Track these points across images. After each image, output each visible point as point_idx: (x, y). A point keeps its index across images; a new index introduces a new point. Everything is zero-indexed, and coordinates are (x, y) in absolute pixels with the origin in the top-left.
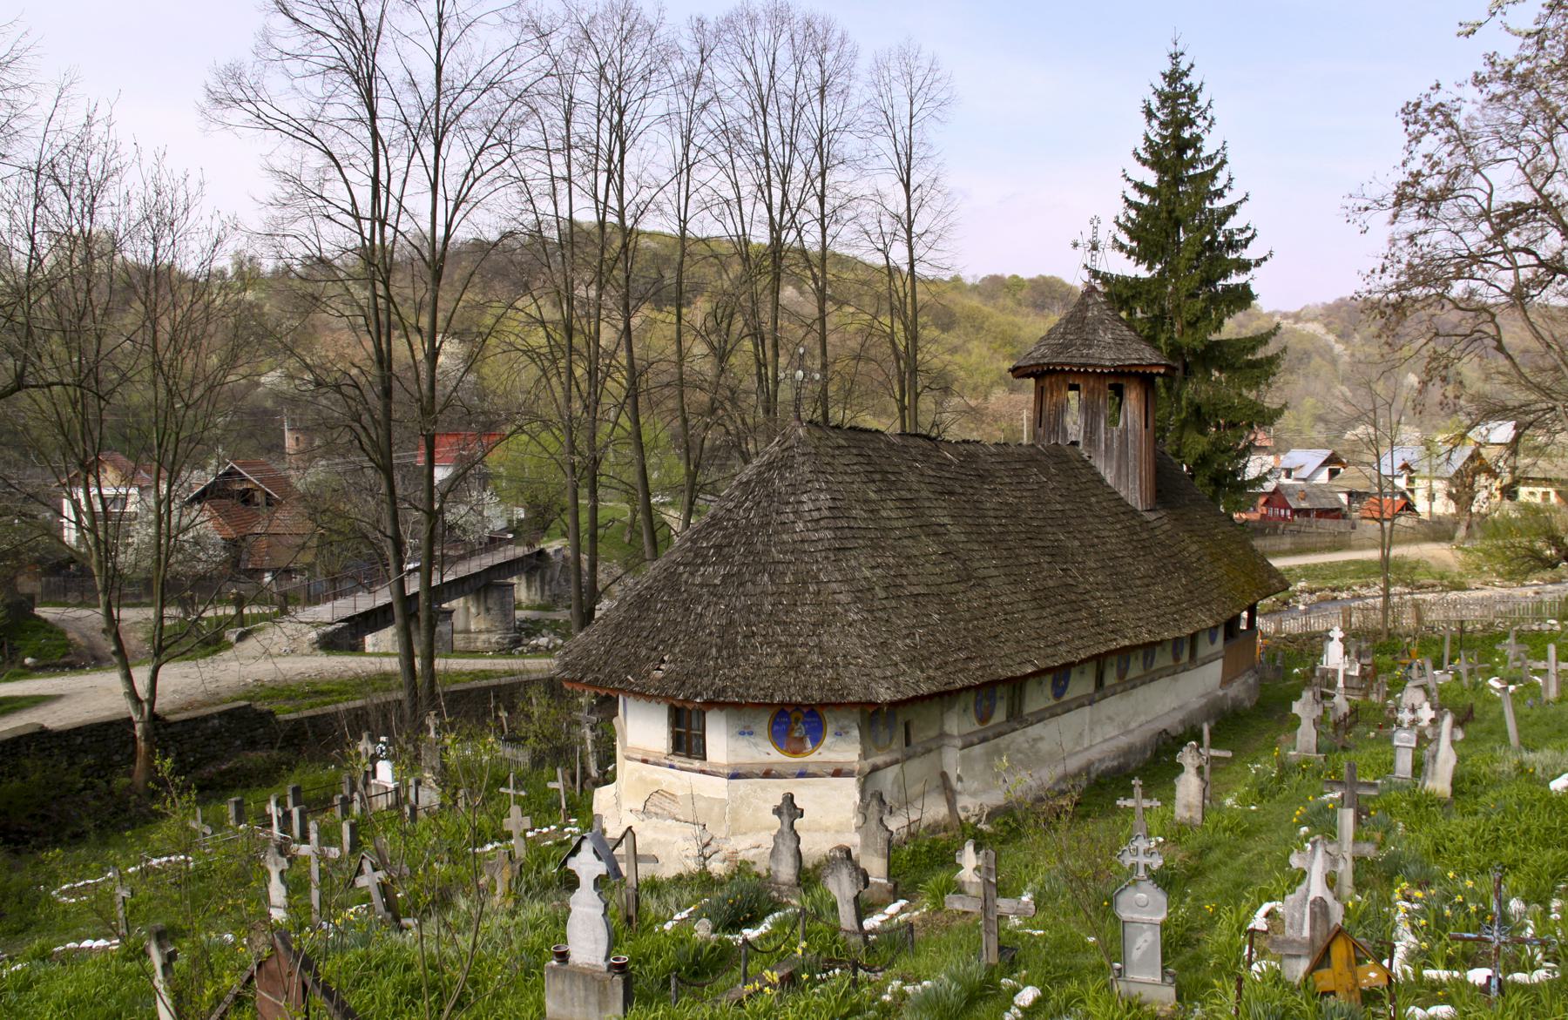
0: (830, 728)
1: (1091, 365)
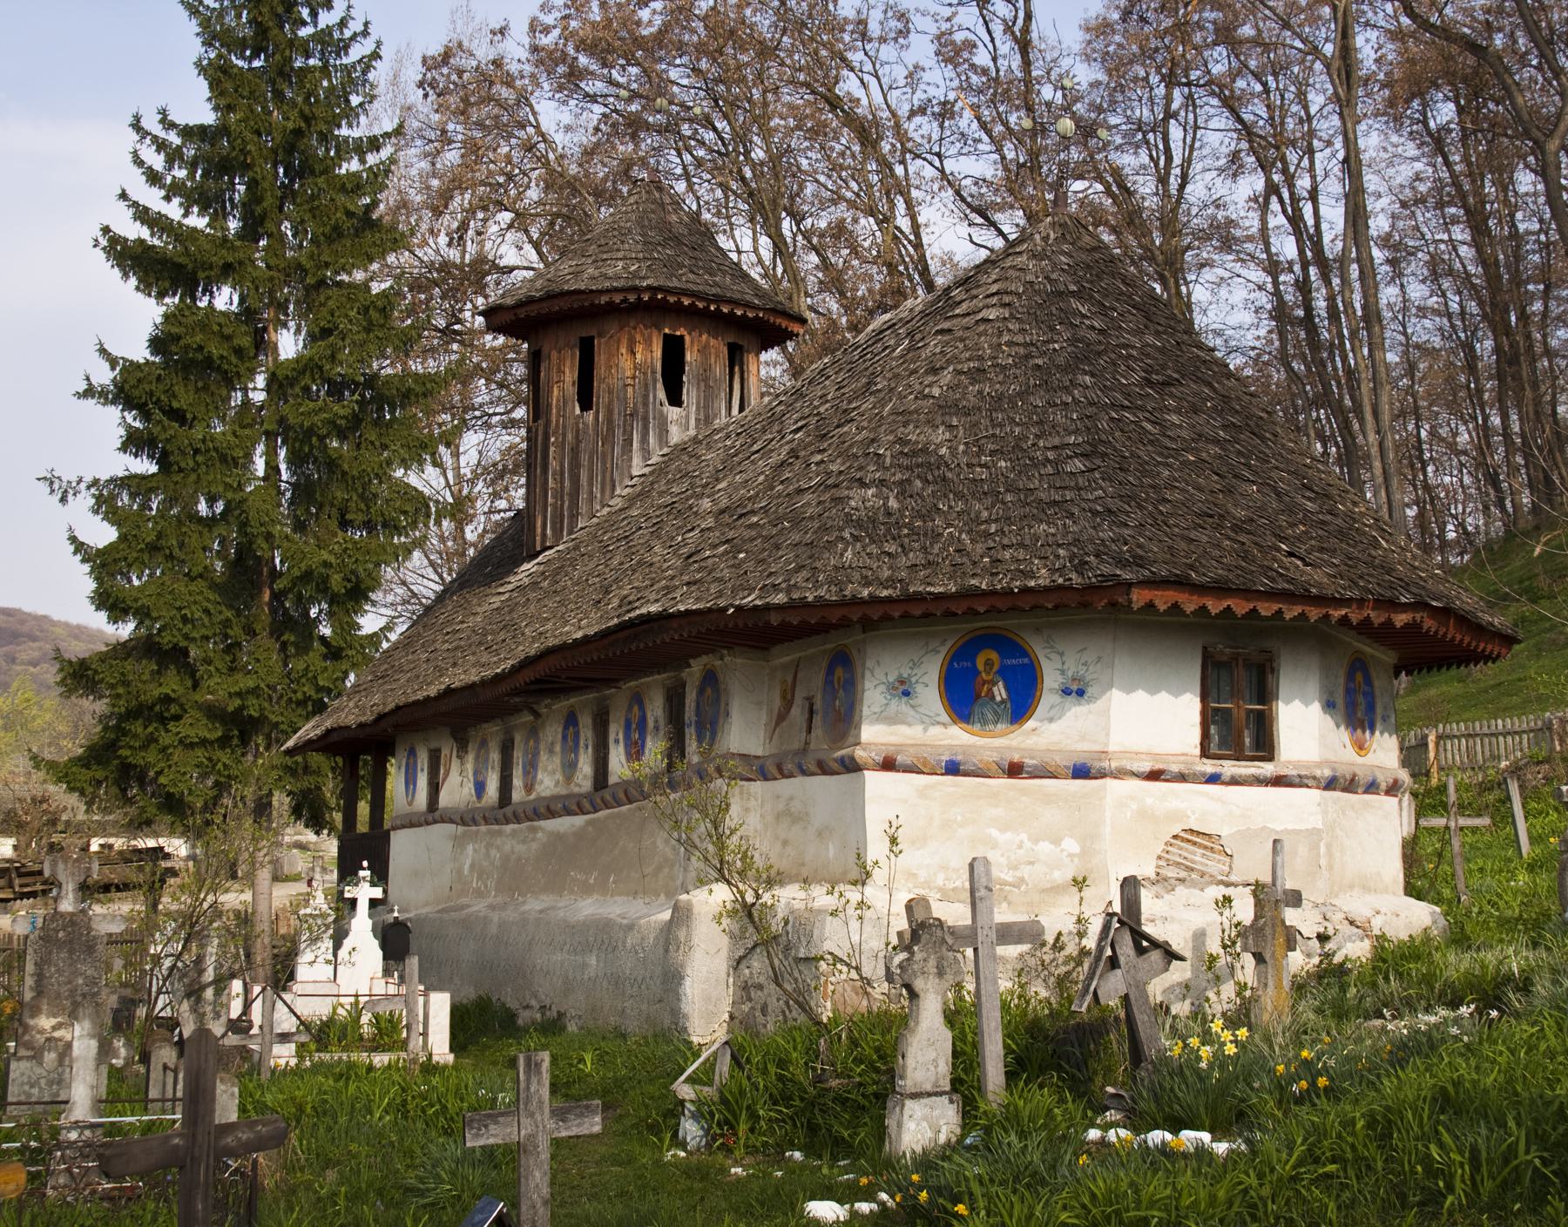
0: (1051, 679)
1: (730, 301)
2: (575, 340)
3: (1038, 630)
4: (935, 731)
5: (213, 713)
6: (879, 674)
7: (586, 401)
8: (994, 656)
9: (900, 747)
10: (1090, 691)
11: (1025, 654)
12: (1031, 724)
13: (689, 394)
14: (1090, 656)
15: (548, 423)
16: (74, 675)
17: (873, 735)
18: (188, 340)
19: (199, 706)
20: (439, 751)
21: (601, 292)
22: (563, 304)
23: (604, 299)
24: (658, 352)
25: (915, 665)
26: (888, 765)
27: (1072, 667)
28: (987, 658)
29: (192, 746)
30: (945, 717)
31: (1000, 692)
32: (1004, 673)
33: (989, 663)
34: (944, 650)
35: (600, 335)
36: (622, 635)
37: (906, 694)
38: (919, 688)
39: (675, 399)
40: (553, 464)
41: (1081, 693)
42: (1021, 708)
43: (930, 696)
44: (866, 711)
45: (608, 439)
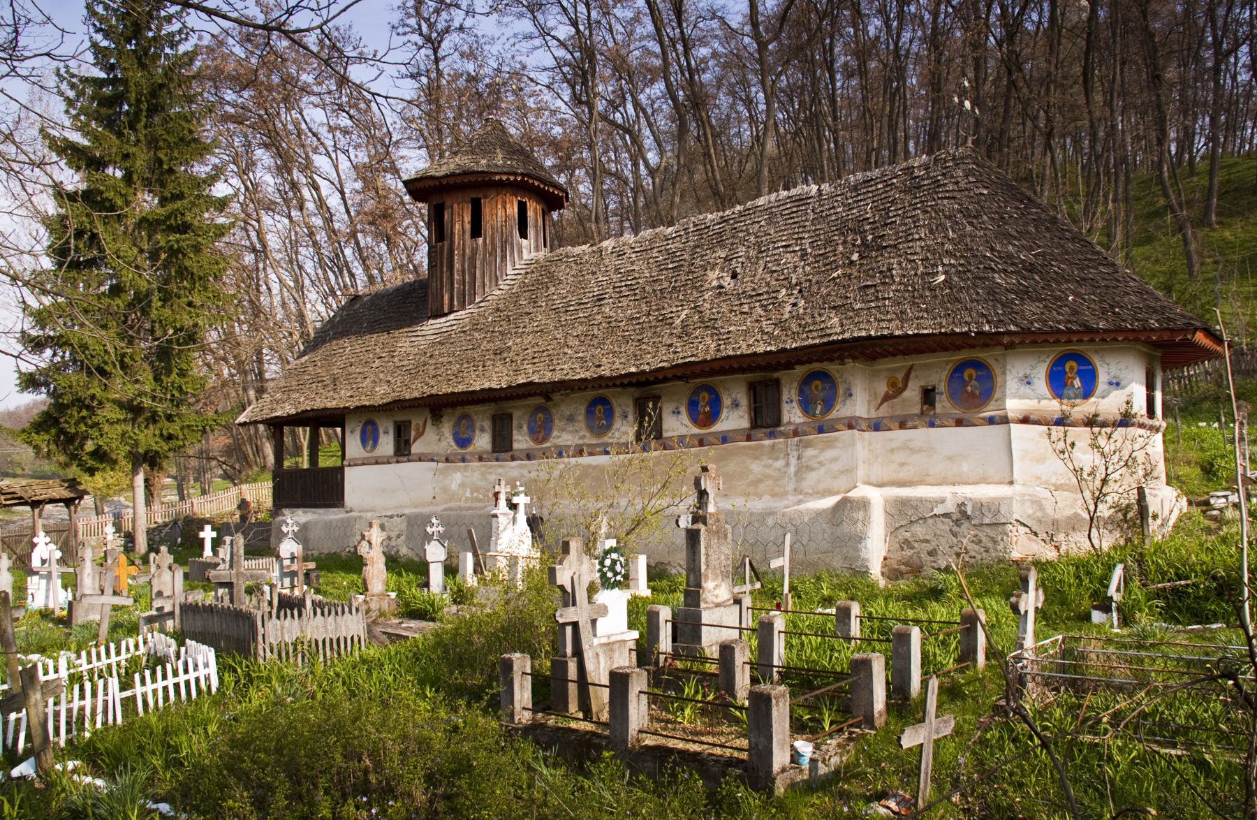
2: (468, 199)
3: (1096, 352)
4: (1044, 403)
5: (120, 404)
6: (1014, 372)
7: (476, 231)
8: (1074, 364)
9: (1031, 412)
10: (1123, 383)
11: (1090, 363)
12: (1092, 400)
13: (531, 232)
14: (1122, 366)
15: (452, 243)
16: (26, 382)
17: (1014, 405)
18: (106, 195)
19: (114, 401)
20: (408, 424)
21: (496, 173)
22: (472, 179)
23: (497, 178)
24: (516, 210)
25: (1033, 368)
26: (1025, 420)
27: (1114, 372)
28: (1070, 365)
29: (112, 423)
30: (1049, 395)
31: (1077, 383)
32: (1080, 373)
33: (1071, 368)
34: (1048, 361)
35: (485, 197)
36: (867, 343)
37: (1029, 383)
38: (1035, 380)
39: (524, 235)
40: (457, 266)
41: (1118, 384)
42: (1087, 393)
43: (1041, 385)
44: (1008, 392)
45: (493, 253)
